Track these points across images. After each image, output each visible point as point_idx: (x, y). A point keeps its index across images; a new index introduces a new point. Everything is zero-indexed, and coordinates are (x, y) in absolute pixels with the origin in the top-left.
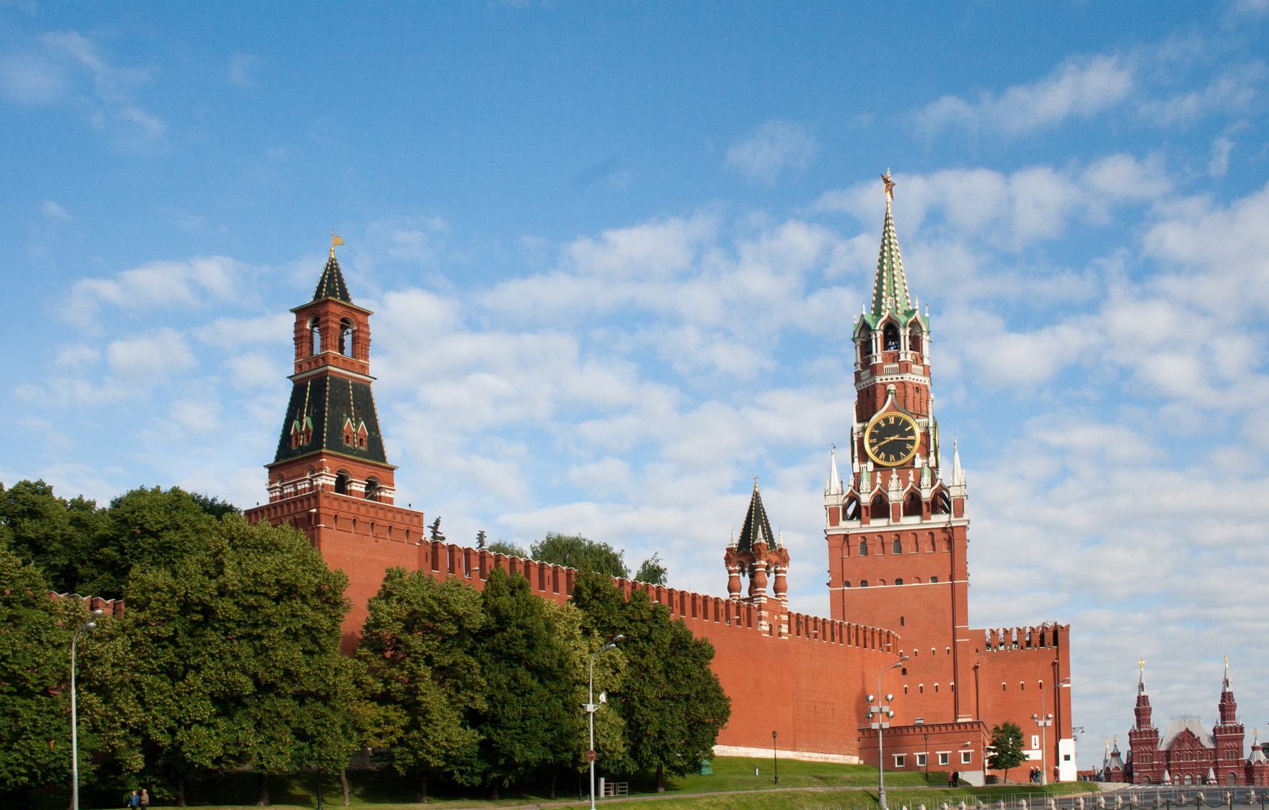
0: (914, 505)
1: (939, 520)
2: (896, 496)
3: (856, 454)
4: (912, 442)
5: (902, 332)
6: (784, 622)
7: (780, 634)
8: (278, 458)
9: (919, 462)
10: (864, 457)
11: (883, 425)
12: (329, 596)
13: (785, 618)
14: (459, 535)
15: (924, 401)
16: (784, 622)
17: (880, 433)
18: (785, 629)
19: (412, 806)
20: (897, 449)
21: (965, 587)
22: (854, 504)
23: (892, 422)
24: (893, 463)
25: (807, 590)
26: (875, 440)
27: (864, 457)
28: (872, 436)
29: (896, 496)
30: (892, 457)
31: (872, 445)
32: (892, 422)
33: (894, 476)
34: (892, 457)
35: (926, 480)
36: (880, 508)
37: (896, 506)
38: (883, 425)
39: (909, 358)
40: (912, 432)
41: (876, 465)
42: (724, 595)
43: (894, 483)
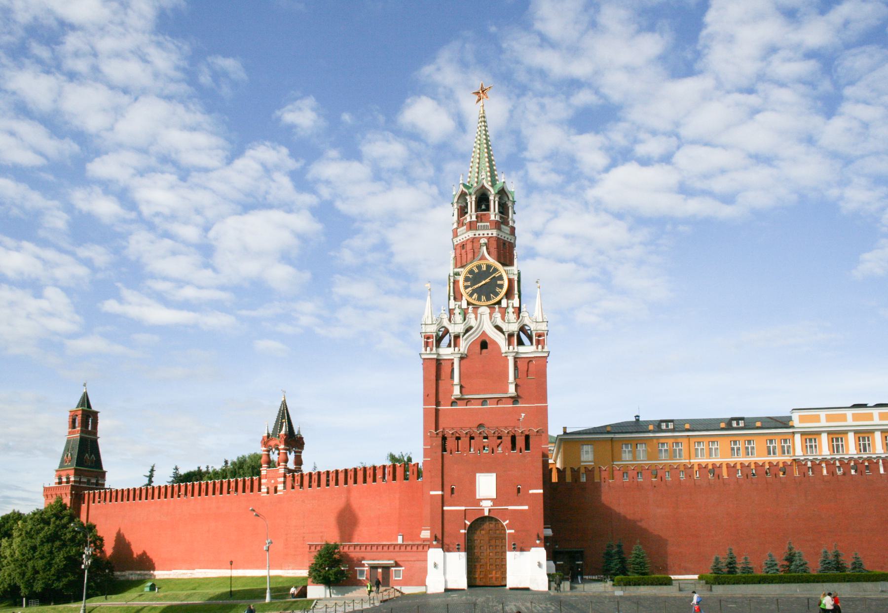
3: (452, 294)
4: (466, 287)
5: (491, 198)
8: (60, 467)
9: (504, 303)
10: (457, 297)
11: (476, 271)
12: (66, 504)
14: (533, 549)
15: (459, 259)
17: (474, 277)
19: (61, 607)
21: (426, 402)
23: (484, 268)
24: (484, 301)
26: (469, 283)
27: (457, 297)
28: (466, 279)
30: (483, 298)
31: (466, 287)
32: (484, 268)
34: (483, 298)
38: (476, 271)
39: (474, 218)
40: (501, 278)
41: (469, 304)
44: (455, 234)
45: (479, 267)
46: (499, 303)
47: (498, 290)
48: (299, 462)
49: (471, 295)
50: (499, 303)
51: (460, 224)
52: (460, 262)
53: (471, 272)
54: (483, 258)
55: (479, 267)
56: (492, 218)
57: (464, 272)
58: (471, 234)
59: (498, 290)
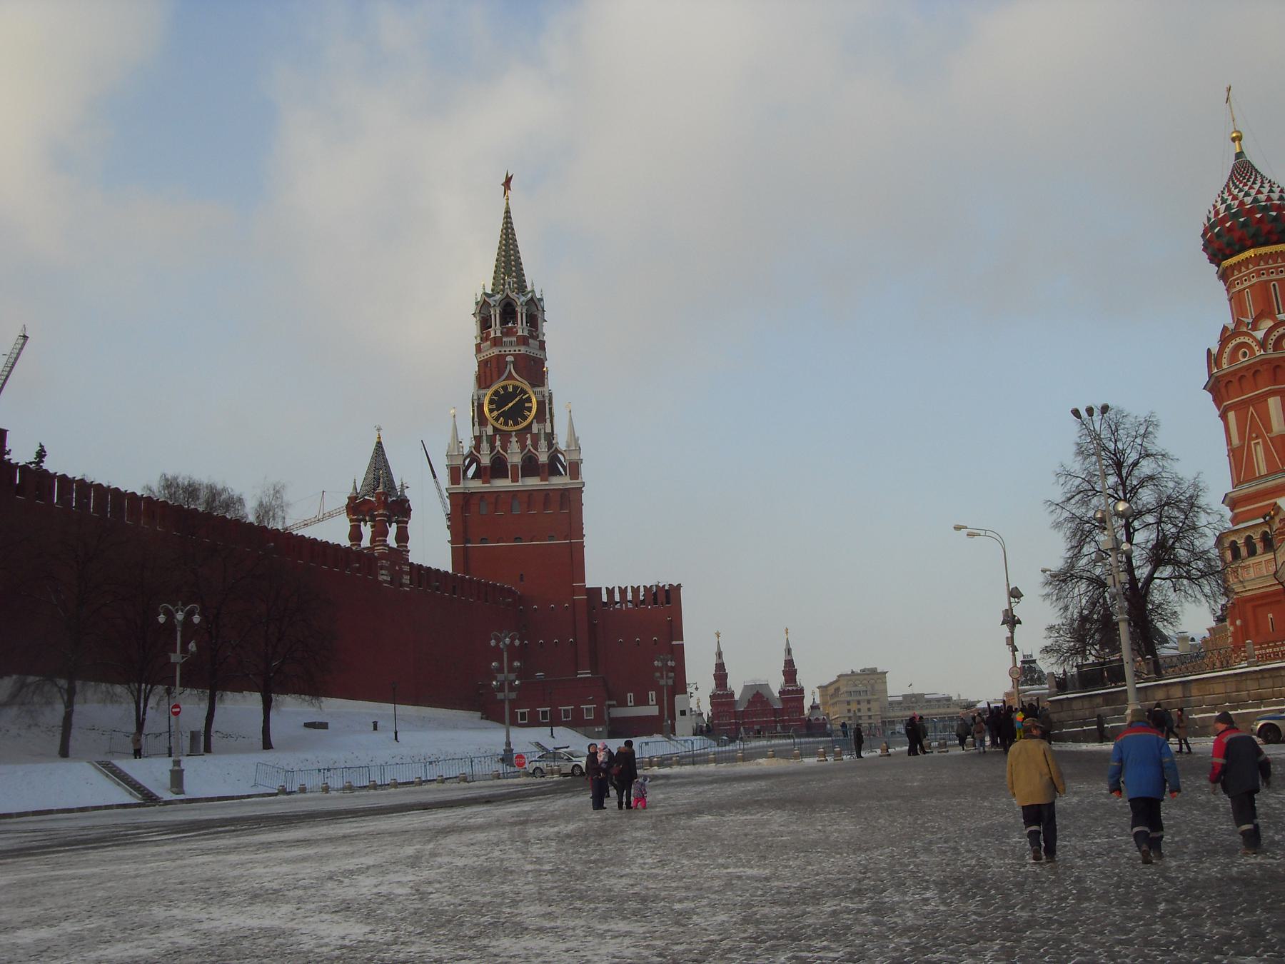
0: (530, 466)
1: (557, 482)
2: (514, 456)
5: (519, 309)
6: (406, 573)
7: (402, 585)
9: (535, 429)
13: (407, 568)
16: (406, 573)
17: (499, 400)
18: (406, 579)
20: (518, 413)
22: (474, 465)
25: (431, 543)
28: (491, 402)
29: (514, 456)
30: (511, 422)
31: (491, 411)
33: (514, 439)
34: (511, 422)
35: (543, 444)
36: (498, 468)
37: (514, 467)
39: (499, 334)
40: (529, 400)
42: (346, 543)
43: (514, 446)
44: (479, 348)
45: (505, 388)
46: (529, 426)
47: (526, 413)
48: (403, 537)
49: (497, 419)
50: (529, 426)
51: (484, 338)
52: (483, 379)
53: (496, 393)
54: (510, 377)
55: (505, 388)
56: (520, 333)
57: (489, 392)
58: (496, 351)
59: (526, 413)
